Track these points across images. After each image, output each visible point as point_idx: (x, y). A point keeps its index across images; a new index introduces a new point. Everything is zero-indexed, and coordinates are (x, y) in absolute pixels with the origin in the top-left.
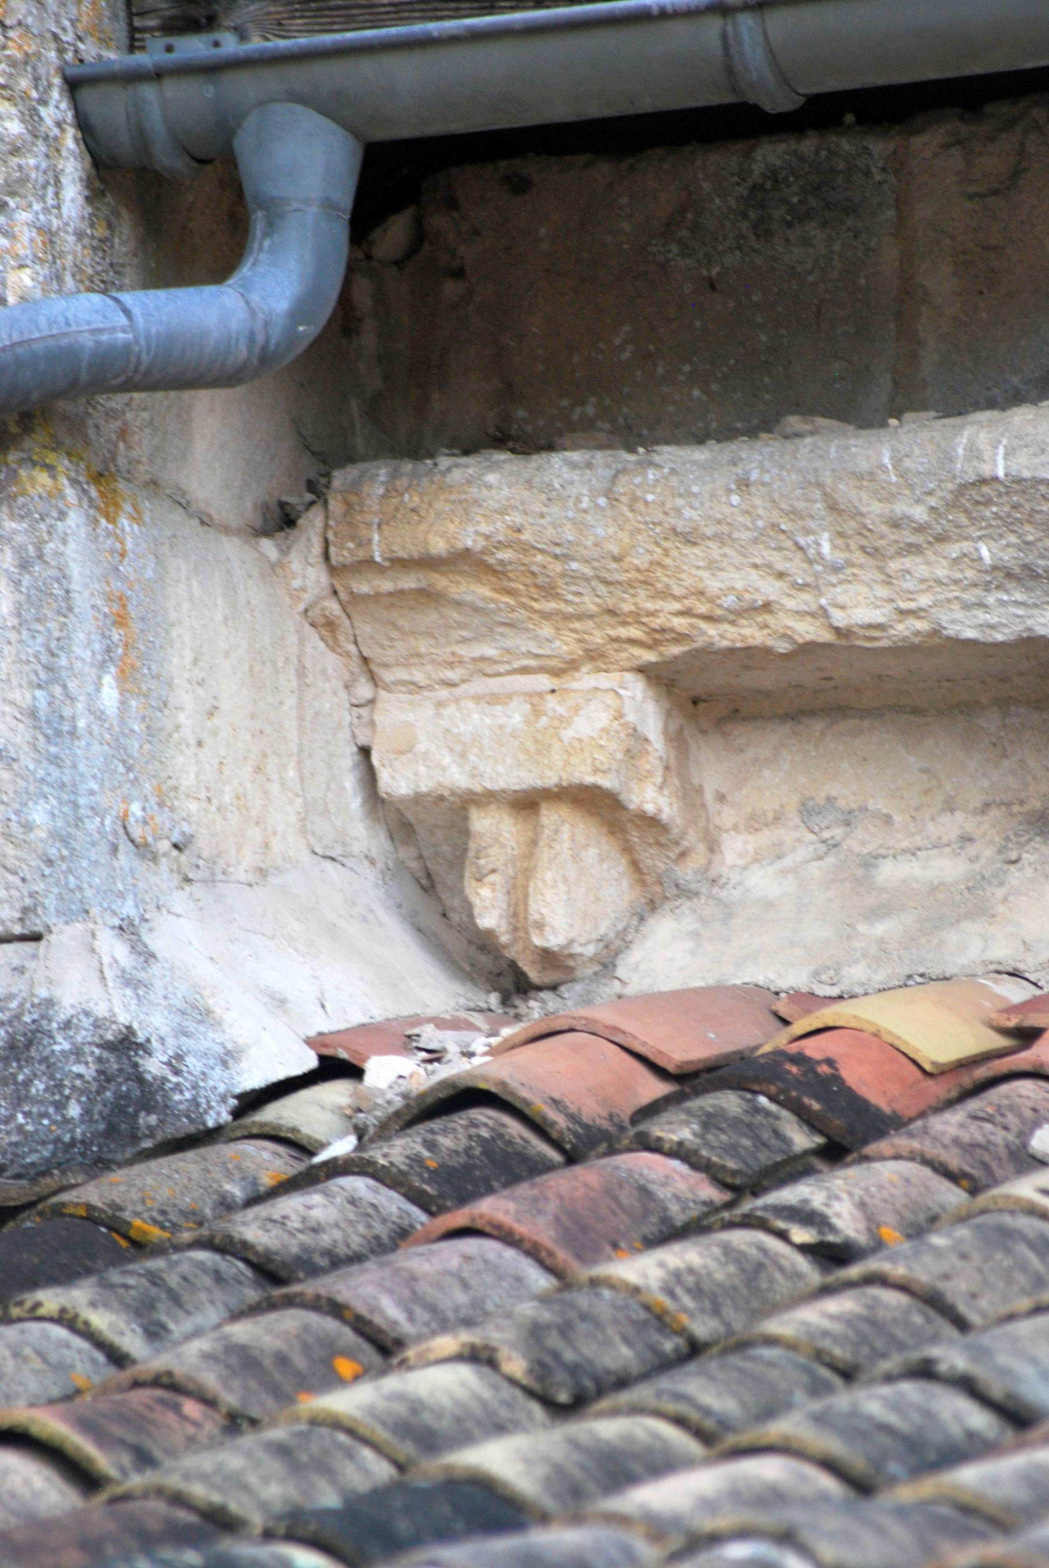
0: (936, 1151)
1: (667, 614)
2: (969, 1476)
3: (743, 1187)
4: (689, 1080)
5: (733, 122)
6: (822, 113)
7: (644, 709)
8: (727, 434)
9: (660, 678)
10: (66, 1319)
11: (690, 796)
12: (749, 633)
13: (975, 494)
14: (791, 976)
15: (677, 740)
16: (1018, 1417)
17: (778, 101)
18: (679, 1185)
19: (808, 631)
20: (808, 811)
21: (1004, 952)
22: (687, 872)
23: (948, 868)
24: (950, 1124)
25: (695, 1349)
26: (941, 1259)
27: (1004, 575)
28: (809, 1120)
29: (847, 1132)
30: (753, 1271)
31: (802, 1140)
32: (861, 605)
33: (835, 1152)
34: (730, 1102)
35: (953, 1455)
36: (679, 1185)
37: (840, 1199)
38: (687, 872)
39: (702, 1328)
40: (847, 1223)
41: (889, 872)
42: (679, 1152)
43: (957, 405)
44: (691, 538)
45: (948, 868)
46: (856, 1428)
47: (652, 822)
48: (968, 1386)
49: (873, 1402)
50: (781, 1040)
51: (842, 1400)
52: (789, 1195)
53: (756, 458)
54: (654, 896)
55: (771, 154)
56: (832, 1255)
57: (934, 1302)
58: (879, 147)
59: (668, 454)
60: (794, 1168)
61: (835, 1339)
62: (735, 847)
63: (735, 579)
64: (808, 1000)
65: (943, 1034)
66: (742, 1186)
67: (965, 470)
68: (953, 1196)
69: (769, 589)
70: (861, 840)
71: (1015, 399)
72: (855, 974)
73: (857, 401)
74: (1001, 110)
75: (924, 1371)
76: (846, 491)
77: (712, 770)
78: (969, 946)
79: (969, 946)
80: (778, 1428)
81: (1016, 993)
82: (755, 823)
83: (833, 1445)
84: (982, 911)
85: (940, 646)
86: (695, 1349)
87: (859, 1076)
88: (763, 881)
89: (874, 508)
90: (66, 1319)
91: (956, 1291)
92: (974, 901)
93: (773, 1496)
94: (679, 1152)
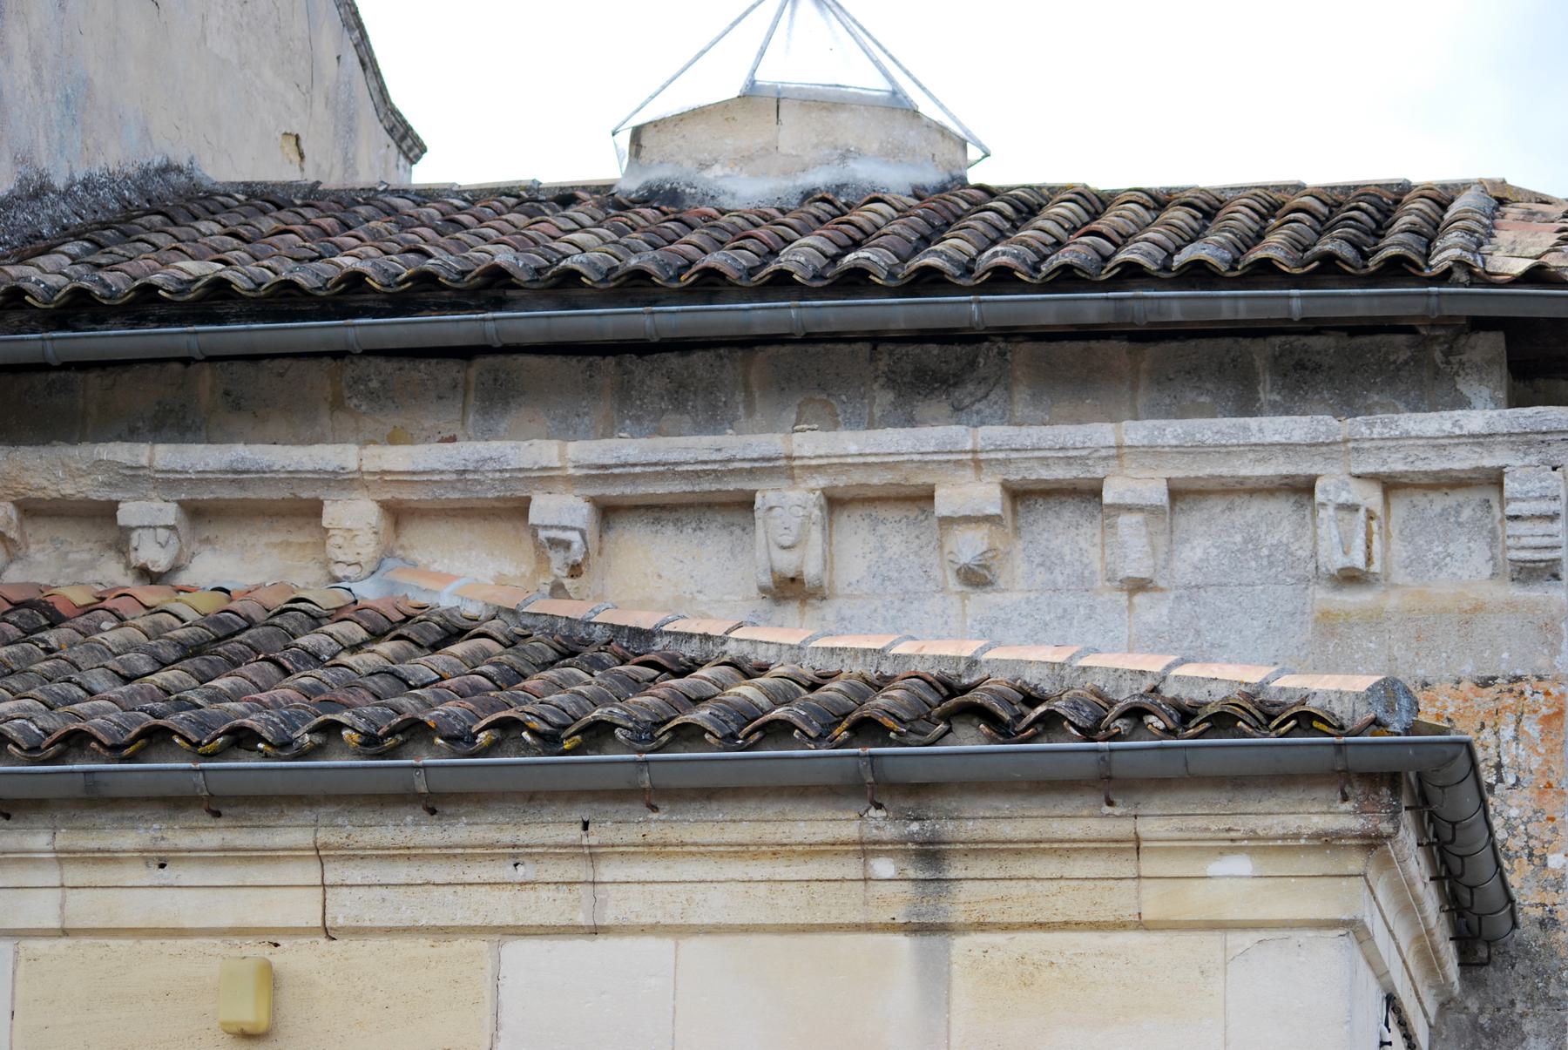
0: (1074, 473)
1: (20, 488)
2: (77, 706)
3: (29, 633)
4: (17, 605)
5: (43, 367)
6: (66, 366)
7: (11, 510)
8: (37, 444)
9: (17, 504)
10: (1146, 240)
11: (23, 534)
12: (40, 494)
13: (98, 464)
14: (45, 582)
15: (20, 520)
16: (91, 693)
17: (55, 363)
18: (12, 631)
19: (55, 495)
20: (52, 540)
21: (99, 578)
22: (20, 554)
23: (86, 556)
24: (81, 620)
25: (13, 672)
26: (74, 654)
27: (104, 484)
28: (47, 617)
29: (55, 620)
30: (29, 653)
31: (44, 622)
32: (68, 489)
33: (52, 626)
34: (27, 611)
35: (74, 702)
36: (12, 631)
37: (52, 637)
38: (20, 554)
39: (15, 667)
40: (53, 643)
41: (71, 556)
42: (13, 623)
43: (96, 441)
44: (27, 470)
45: (86, 556)
46: (51, 694)
47: (12, 540)
48: (79, 685)
49: (55, 687)
50: (41, 597)
51: (47, 687)
52: (39, 635)
53: (45, 451)
54: (12, 559)
55: (53, 375)
56: (49, 651)
57: (73, 664)
58: (80, 376)
59: (22, 448)
60: (42, 629)
61: (902, 707)
62: (33, 548)
63: (37, 480)
64: (49, 587)
65: (81, 598)
66: (28, 633)
67: (96, 457)
68: (81, 638)
69: (46, 484)
70: (65, 548)
71: (110, 440)
72: (61, 581)
73: (70, 439)
74: (110, 369)
75: (69, 681)
76: (66, 460)
77: (28, 529)
78: (90, 576)
79: (90, 576)
80: (30, 693)
81: (100, 588)
82: (38, 542)
83: (44, 698)
84: (93, 568)
85: (88, 501)
86: (13, 672)
87: (60, 607)
88: (39, 557)
89: (73, 465)
90: (1146, 240)
91: (79, 661)
92: (91, 565)
93: (29, 709)
94: (13, 623)
